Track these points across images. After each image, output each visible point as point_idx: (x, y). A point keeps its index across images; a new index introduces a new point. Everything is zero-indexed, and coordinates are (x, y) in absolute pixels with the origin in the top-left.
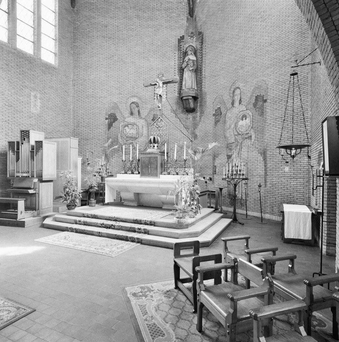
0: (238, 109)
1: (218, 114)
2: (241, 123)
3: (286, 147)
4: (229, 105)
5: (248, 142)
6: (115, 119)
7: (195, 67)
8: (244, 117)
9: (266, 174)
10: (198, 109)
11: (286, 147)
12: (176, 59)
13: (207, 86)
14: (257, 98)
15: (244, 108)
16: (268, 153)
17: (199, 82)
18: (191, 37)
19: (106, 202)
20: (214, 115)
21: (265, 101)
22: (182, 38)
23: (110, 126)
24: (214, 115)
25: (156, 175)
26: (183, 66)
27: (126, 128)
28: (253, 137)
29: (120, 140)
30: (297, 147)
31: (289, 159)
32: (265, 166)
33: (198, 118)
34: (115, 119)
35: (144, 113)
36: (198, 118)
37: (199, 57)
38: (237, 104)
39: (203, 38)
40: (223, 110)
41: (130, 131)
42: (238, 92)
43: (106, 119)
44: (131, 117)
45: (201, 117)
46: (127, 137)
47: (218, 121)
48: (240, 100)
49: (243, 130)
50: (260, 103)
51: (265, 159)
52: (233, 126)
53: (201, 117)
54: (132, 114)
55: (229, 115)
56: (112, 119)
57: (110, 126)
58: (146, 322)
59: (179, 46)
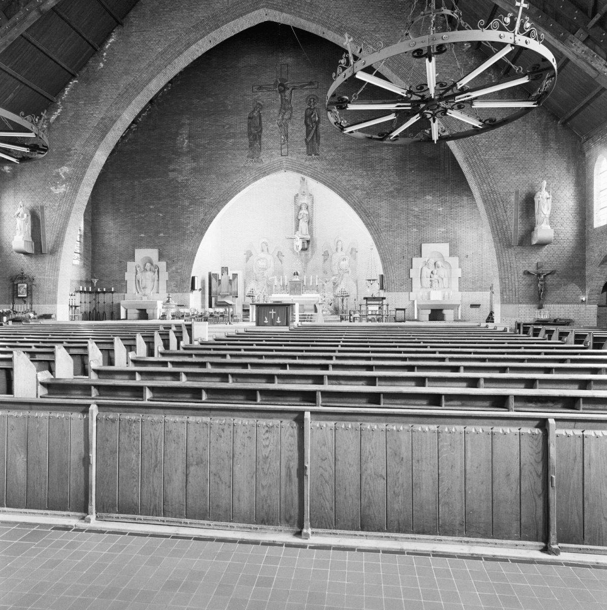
0: (340, 254)
1: (326, 255)
2: (342, 263)
3: (369, 280)
4: (334, 251)
5: (346, 275)
6: (251, 255)
7: (308, 220)
8: (344, 259)
9: (357, 294)
10: (310, 249)
11: (369, 280)
12: (293, 211)
13: (317, 234)
14: (352, 249)
15: (344, 254)
16: (359, 282)
17: (311, 231)
18: (303, 195)
19: (121, 318)
20: (323, 255)
21: (357, 252)
22: (297, 195)
23: (247, 259)
24: (323, 255)
25: (300, 294)
26: (299, 217)
27: (259, 261)
28: (350, 272)
29: (255, 271)
30: (374, 280)
31: (369, 285)
32: (357, 289)
33: (310, 256)
34: (251, 255)
35: (271, 251)
36: (310, 256)
37: (310, 211)
38: (339, 250)
39: (313, 200)
40: (330, 253)
41: (262, 264)
42: (340, 243)
43: (245, 254)
44: (262, 253)
45: (312, 255)
46: (260, 268)
47: (326, 260)
48: (342, 248)
49: (344, 267)
50: (354, 253)
51: (357, 285)
52: (337, 264)
53: (312, 255)
54: (263, 251)
55: (334, 256)
56: (249, 255)
57: (247, 259)
58: (221, 426)
59: (295, 201)
